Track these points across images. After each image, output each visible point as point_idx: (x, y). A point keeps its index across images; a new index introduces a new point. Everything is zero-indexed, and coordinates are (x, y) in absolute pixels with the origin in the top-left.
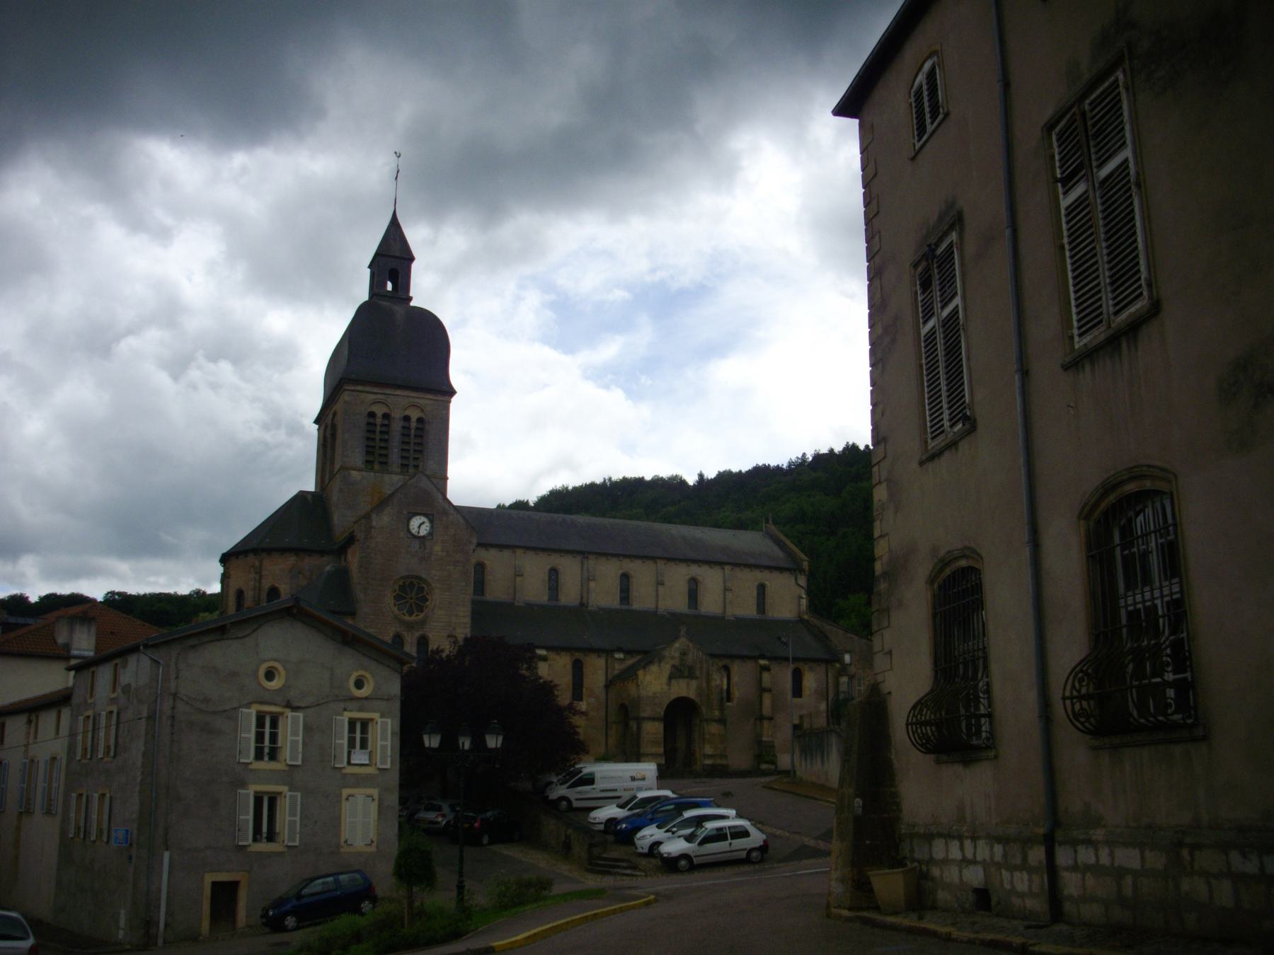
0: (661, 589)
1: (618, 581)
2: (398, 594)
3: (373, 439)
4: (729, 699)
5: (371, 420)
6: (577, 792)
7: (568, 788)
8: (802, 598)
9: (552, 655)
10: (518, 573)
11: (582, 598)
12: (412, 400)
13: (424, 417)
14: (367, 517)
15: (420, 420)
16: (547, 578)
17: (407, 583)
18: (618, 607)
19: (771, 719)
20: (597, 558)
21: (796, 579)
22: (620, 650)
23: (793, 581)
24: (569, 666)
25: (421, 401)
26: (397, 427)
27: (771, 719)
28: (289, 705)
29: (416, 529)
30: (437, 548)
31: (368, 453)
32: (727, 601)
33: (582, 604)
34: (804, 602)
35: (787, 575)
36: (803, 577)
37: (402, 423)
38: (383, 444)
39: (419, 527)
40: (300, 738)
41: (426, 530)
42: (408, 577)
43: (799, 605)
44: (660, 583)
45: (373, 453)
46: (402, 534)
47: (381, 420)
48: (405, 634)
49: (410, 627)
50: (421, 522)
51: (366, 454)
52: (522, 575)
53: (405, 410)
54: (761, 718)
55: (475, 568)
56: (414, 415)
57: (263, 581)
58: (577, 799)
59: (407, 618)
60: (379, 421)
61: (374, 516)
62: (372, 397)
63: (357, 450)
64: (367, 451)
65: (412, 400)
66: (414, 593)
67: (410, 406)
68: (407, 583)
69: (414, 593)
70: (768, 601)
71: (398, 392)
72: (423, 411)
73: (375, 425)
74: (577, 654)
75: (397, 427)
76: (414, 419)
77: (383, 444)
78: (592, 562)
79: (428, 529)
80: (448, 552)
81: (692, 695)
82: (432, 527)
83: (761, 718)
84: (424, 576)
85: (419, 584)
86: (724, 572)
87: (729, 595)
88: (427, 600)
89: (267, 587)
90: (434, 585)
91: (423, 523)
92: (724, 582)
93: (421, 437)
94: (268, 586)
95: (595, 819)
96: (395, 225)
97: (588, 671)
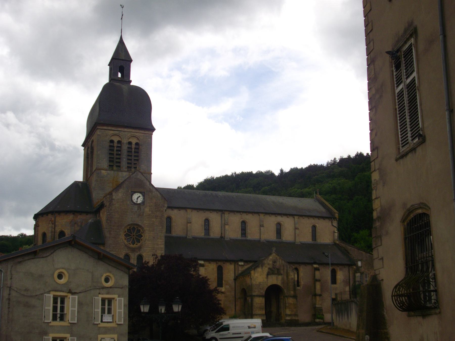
0: (262, 228)
2: (126, 233)
4: (298, 285)
5: (112, 144)
7: (216, 332)
8: (335, 232)
9: (207, 264)
10: (188, 222)
11: (222, 234)
12: (132, 134)
14: (110, 194)
15: (137, 144)
16: (203, 224)
17: (131, 228)
18: (240, 238)
19: (320, 295)
20: (229, 213)
21: (332, 223)
22: (241, 260)
23: (330, 224)
24: (216, 269)
25: (137, 134)
26: (125, 147)
27: (320, 295)
28: (70, 292)
29: (136, 200)
30: (147, 209)
31: (110, 161)
32: (297, 235)
33: (222, 237)
34: (336, 234)
35: (327, 220)
36: (335, 221)
37: (127, 146)
38: (118, 157)
39: (137, 199)
40: (76, 309)
42: (132, 224)
43: (334, 236)
44: (262, 226)
45: (113, 161)
48: (130, 254)
49: (133, 250)
50: (138, 196)
51: (109, 162)
52: (191, 223)
53: (129, 139)
54: (315, 295)
56: (134, 141)
57: (56, 228)
59: (132, 246)
61: (114, 194)
63: (104, 160)
64: (109, 160)
65: (132, 134)
66: (135, 232)
67: (131, 137)
68: (131, 228)
69: (135, 232)
70: (318, 234)
71: (126, 130)
72: (138, 139)
75: (125, 147)
76: (134, 143)
77: (118, 157)
78: (226, 215)
79: (142, 199)
80: (152, 211)
81: (279, 283)
82: (144, 199)
83: (315, 295)
84: (140, 224)
85: (137, 228)
86: (295, 219)
87: (297, 231)
88: (142, 236)
89: (58, 231)
90: (145, 229)
91: (139, 197)
92: (295, 225)
93: (138, 152)
97: (225, 272)
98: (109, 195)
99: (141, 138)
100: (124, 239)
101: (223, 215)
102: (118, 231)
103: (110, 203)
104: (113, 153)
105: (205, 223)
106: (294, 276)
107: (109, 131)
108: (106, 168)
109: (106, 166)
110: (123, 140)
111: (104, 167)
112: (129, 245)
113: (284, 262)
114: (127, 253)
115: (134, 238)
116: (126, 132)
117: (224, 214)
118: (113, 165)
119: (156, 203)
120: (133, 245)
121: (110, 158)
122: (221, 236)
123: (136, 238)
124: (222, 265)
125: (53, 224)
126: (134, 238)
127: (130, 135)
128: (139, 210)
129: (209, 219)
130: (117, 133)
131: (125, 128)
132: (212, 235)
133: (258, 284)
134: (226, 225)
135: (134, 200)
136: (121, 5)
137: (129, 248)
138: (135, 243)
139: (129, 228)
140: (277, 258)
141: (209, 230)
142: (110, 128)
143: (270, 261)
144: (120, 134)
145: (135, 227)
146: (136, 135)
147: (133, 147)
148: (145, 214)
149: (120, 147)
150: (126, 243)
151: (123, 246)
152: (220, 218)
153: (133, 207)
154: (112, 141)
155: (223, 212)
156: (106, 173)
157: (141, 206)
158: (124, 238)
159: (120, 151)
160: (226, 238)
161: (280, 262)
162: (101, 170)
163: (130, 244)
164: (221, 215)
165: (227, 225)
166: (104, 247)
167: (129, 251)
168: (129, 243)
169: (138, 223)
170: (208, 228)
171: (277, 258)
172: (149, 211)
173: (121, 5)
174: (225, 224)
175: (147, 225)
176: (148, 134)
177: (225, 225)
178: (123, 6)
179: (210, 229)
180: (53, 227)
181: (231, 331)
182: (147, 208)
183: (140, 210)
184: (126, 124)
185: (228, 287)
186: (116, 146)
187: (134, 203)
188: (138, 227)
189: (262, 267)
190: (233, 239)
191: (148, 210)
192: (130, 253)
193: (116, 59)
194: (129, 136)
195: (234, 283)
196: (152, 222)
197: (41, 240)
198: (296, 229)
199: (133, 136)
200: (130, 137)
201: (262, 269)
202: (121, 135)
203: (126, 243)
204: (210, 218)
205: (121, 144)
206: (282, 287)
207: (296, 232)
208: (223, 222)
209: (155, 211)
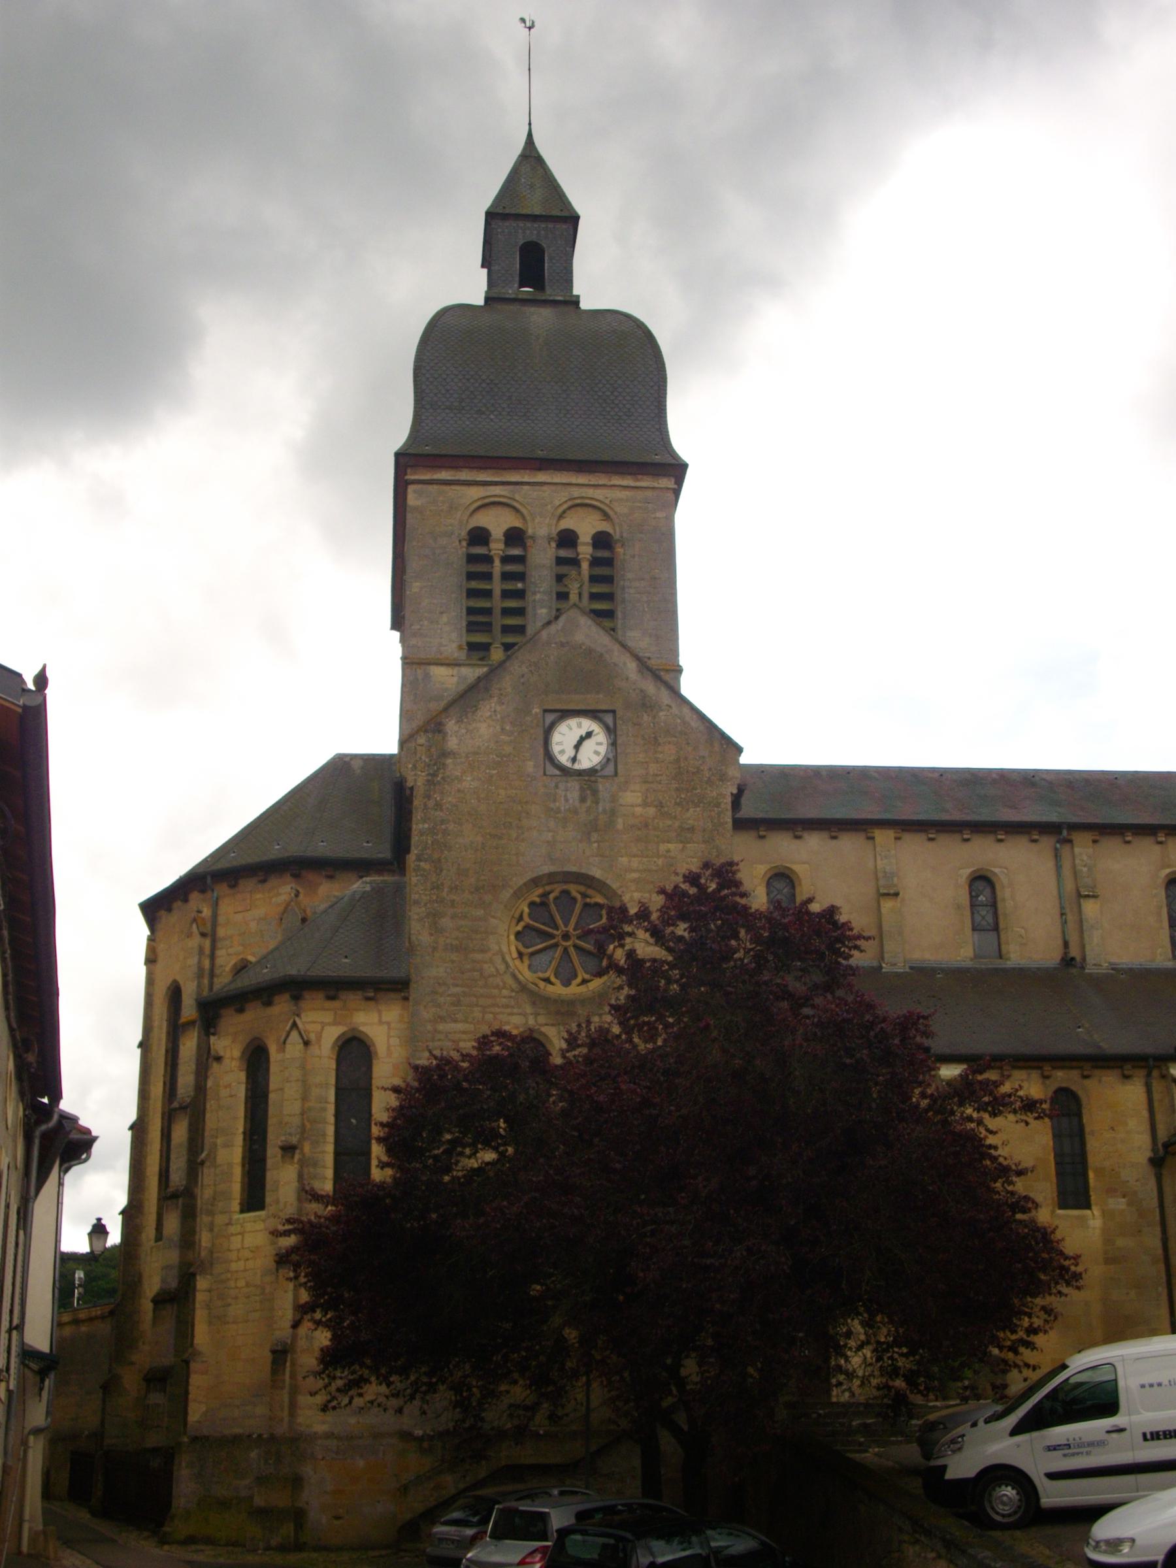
1: (1162, 893)
2: (527, 927)
3: (488, 594)
5: (479, 550)
6: (1054, 1448)
7: (1015, 1432)
10: (882, 891)
11: (1066, 944)
12: (576, 492)
13: (609, 529)
15: (602, 541)
16: (965, 899)
20: (1095, 842)
25: (599, 494)
26: (542, 557)
29: (572, 753)
30: (631, 797)
31: (471, 627)
33: (1068, 961)
38: (512, 604)
39: (577, 747)
41: (597, 753)
42: (551, 878)
45: (487, 627)
46: (530, 767)
47: (501, 546)
50: (583, 732)
52: (896, 894)
53: (561, 517)
55: (769, 884)
56: (586, 527)
57: (219, 953)
58: (1052, 1476)
60: (497, 547)
61: (451, 725)
62: (475, 493)
63: (445, 619)
65: (576, 492)
67: (570, 508)
68: (552, 896)
71: (541, 477)
72: (606, 516)
73: (488, 559)
74: (1060, 1074)
75: (542, 557)
77: (512, 604)
78: (1083, 849)
79: (603, 750)
80: (660, 805)
82: (613, 744)
84: (597, 873)
85: (584, 896)
89: (228, 969)
91: (589, 735)
93: (609, 580)
94: (233, 962)
95: (1114, 1545)
96: (530, 157)
97: (1095, 1119)
98: (426, 731)
99: (618, 509)
100: (515, 955)
101: (1065, 850)
102: (480, 913)
103: (434, 775)
104: (488, 587)
105: (973, 898)
107: (464, 488)
108: (456, 655)
109: (454, 645)
110: (530, 524)
111: (442, 649)
112: (542, 984)
114: (531, 1030)
115: (572, 950)
116: (545, 488)
117: (1072, 848)
118: (490, 641)
119: (678, 761)
120: (567, 983)
121: (470, 611)
122: (1066, 954)
123: (575, 946)
124: (1074, 1088)
125: (203, 935)
126: (572, 950)
127: (566, 502)
128: (589, 803)
129: (995, 874)
130: (503, 493)
131: (540, 469)
132: (1016, 956)
134: (1088, 896)
135: (562, 752)
136: (523, 20)
137: (539, 1000)
138: (576, 976)
139: (538, 900)
141: (996, 928)
142: (464, 475)
144: (517, 497)
145: (574, 894)
146: (601, 498)
147: (581, 556)
148: (620, 820)
149: (521, 559)
150: (526, 975)
151: (505, 992)
152: (1051, 864)
153: (557, 787)
154: (479, 536)
155: (1065, 833)
156: (455, 679)
157: (596, 782)
158: (513, 949)
159: (521, 577)
160: (1095, 965)
162: (429, 664)
163: (547, 980)
164: (1056, 849)
165: (1091, 901)
166: (406, 999)
167: (542, 1019)
168: (541, 975)
169: (583, 871)
170: (991, 921)
172: (645, 804)
173: (523, 20)
174: (1080, 896)
175: (635, 875)
176: (653, 488)
177: (1082, 900)
178: (533, 22)
179: (1001, 925)
180: (207, 951)
181: (1134, 1418)
182: (634, 791)
183: (597, 803)
184: (540, 454)
185: (1118, 1204)
186: (501, 553)
187: (564, 771)
188: (590, 892)
190: (1131, 969)
191: (639, 801)
192: (544, 1029)
193: (505, 217)
194: (560, 505)
195: (1152, 1184)
196: (660, 862)
197: (165, 1024)
199: (578, 501)
200: (565, 506)
202: (521, 504)
203: (526, 975)
204: (996, 870)
205: (524, 546)
208: (1069, 886)
209: (676, 804)
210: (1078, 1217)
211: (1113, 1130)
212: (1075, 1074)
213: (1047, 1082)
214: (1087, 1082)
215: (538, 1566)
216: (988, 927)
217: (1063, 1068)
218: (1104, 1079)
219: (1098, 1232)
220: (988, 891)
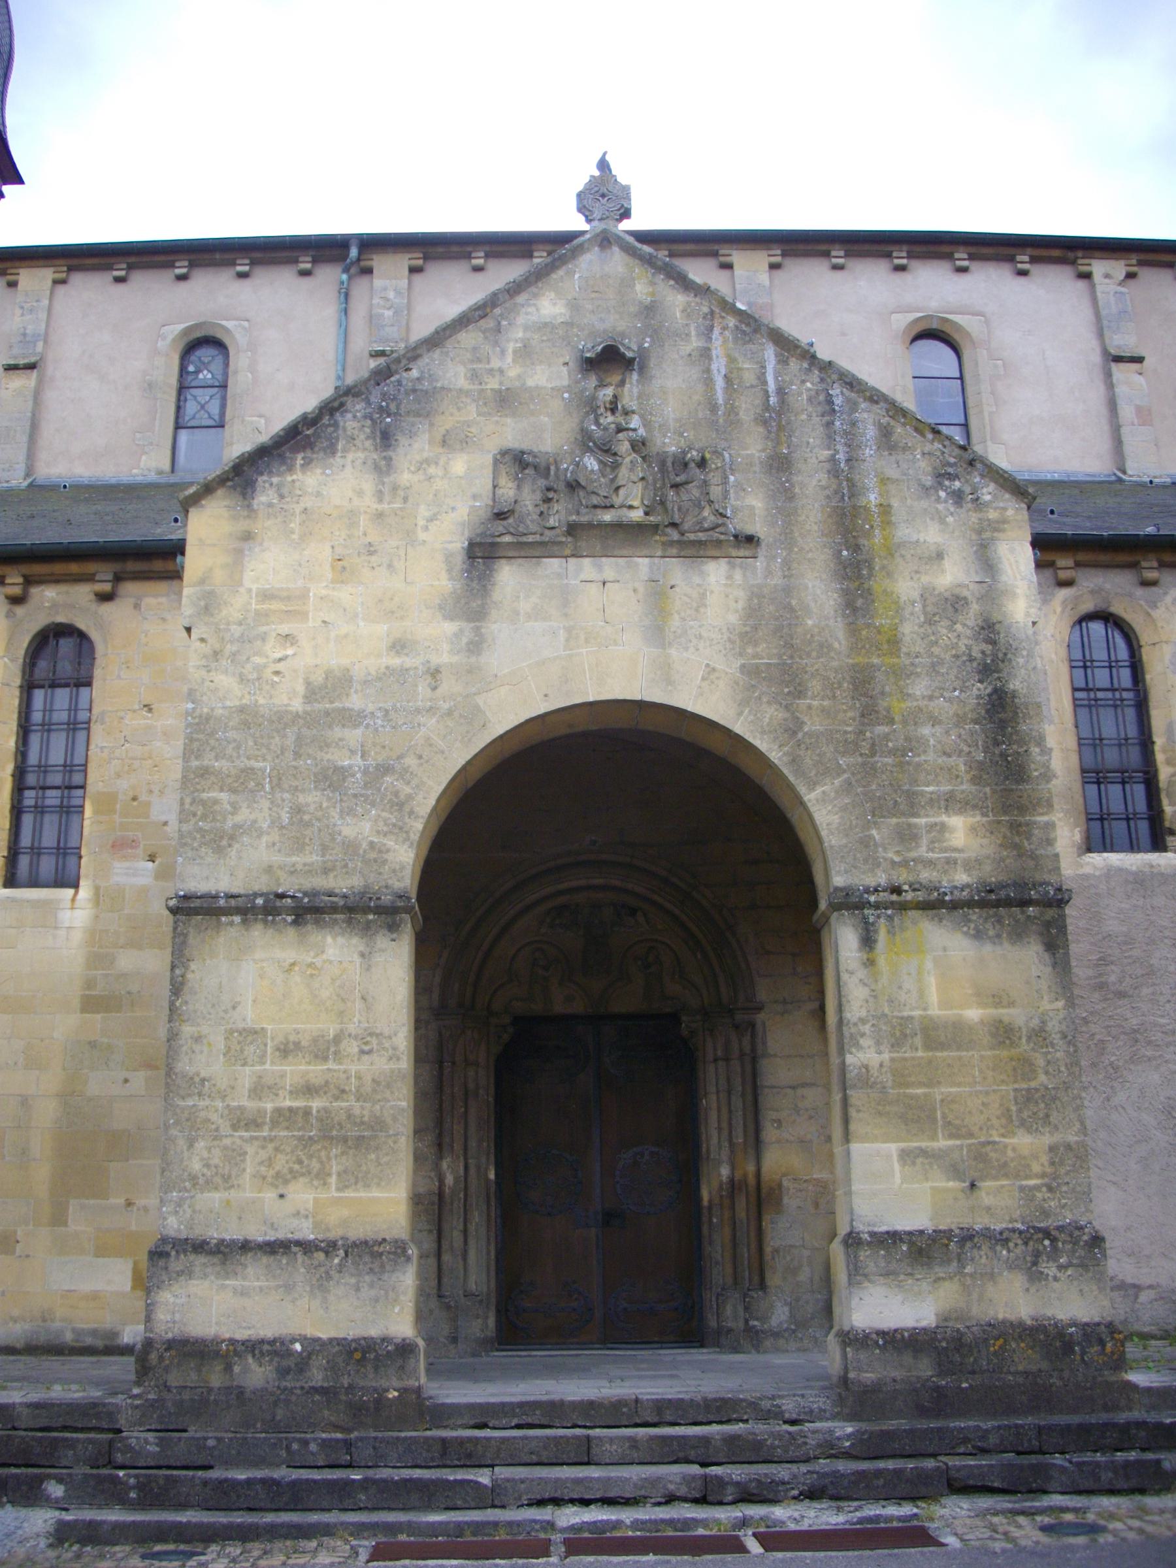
32: (1126, 412)
38: (551, 495)
86: (1093, 287)
92: (1100, 335)
101: (361, 284)
106: (986, 562)
113: (783, 362)
133: (297, 705)
140: (650, 310)
143: (525, 353)
152: (330, 311)
161: (719, 366)
171: (650, 310)
189: (385, 439)
198: (1118, 359)
201: (383, 468)
204: (229, 324)
206: (761, 743)
207: (1121, 390)
210: (36, 904)
211: (150, 710)
212: (83, 593)
213: (20, 611)
214: (106, 608)
215: (223, 1566)
216: (211, 423)
217: (57, 580)
218: (149, 601)
219: (77, 937)
220: (217, 366)
